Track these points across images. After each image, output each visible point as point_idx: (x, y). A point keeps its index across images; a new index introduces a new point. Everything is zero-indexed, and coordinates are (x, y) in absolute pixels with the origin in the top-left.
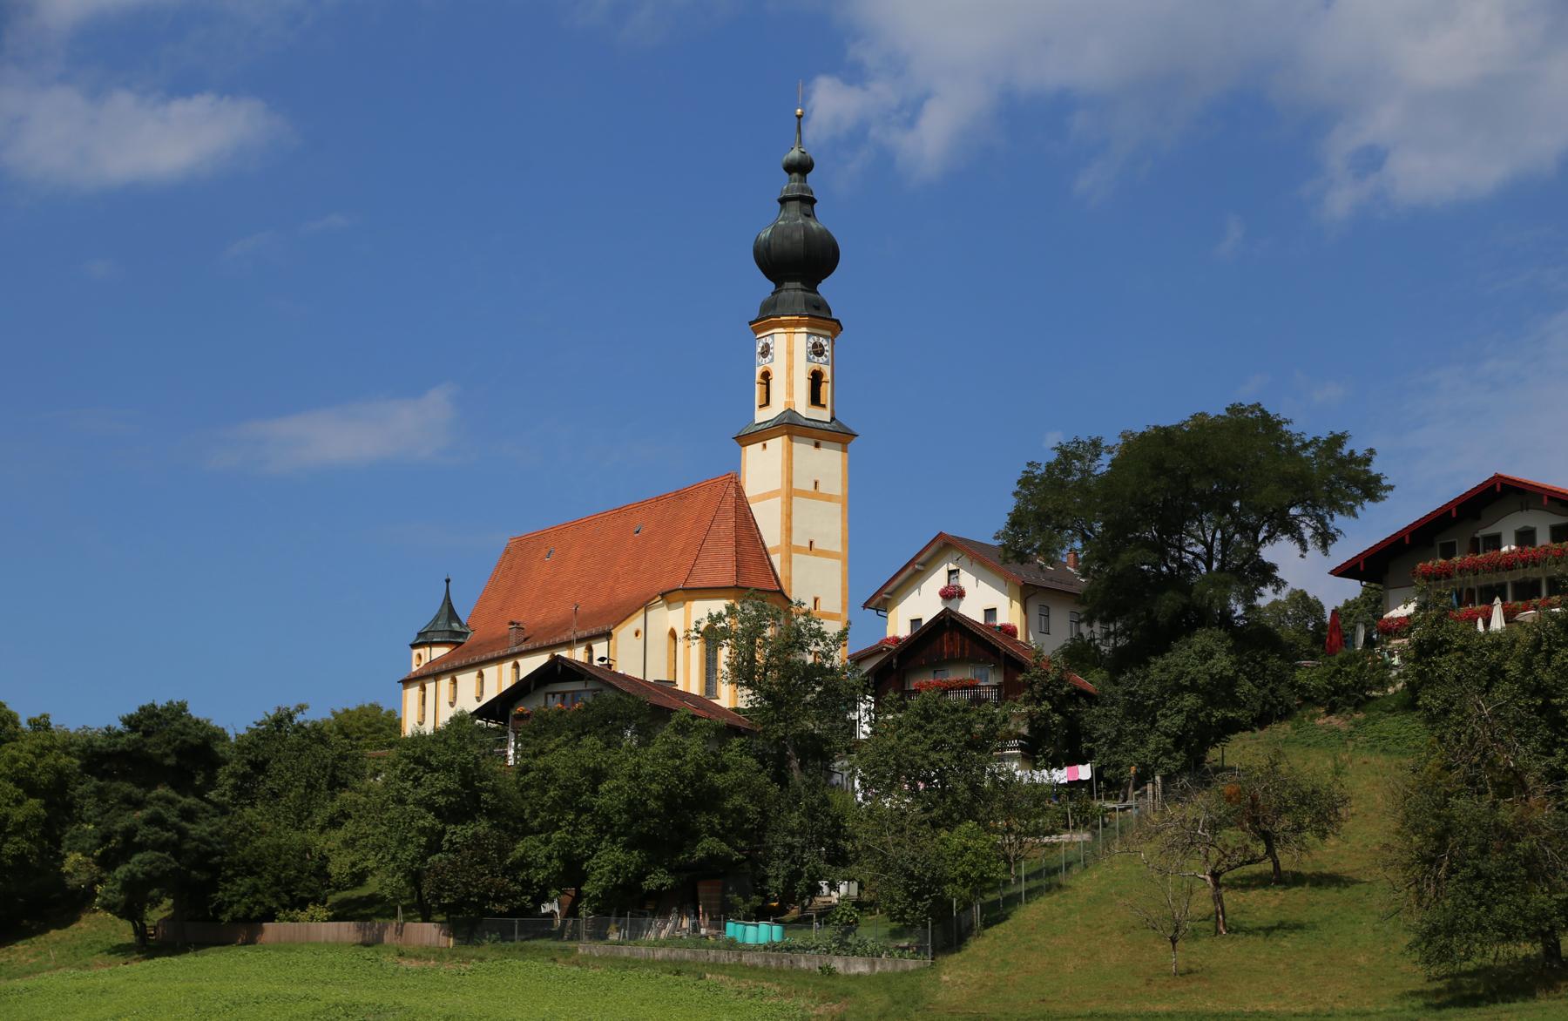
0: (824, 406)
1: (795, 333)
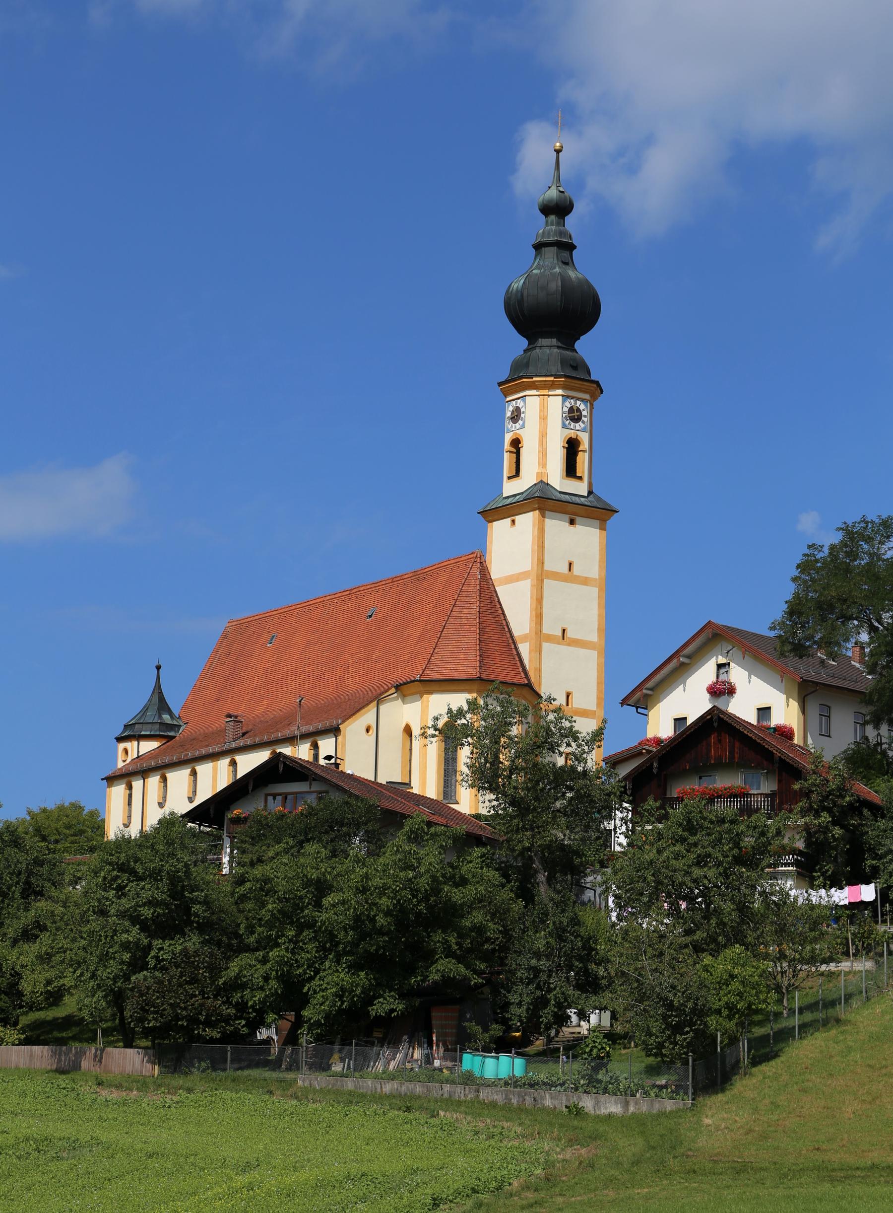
0: (580, 478)
1: (549, 396)
